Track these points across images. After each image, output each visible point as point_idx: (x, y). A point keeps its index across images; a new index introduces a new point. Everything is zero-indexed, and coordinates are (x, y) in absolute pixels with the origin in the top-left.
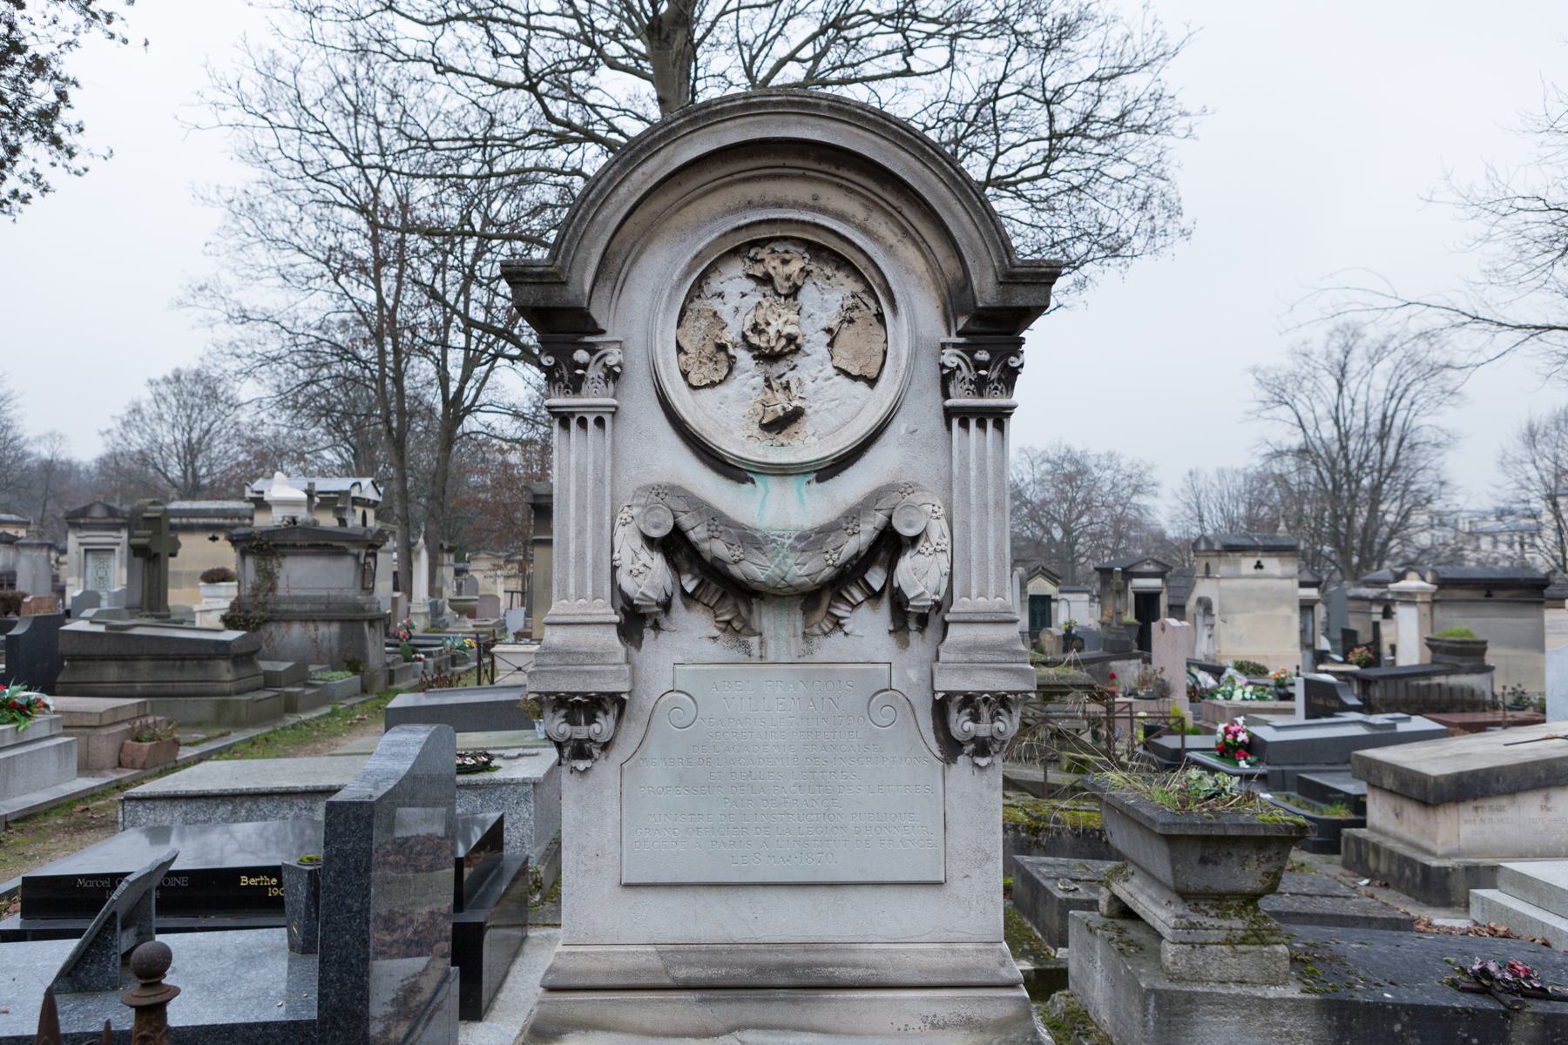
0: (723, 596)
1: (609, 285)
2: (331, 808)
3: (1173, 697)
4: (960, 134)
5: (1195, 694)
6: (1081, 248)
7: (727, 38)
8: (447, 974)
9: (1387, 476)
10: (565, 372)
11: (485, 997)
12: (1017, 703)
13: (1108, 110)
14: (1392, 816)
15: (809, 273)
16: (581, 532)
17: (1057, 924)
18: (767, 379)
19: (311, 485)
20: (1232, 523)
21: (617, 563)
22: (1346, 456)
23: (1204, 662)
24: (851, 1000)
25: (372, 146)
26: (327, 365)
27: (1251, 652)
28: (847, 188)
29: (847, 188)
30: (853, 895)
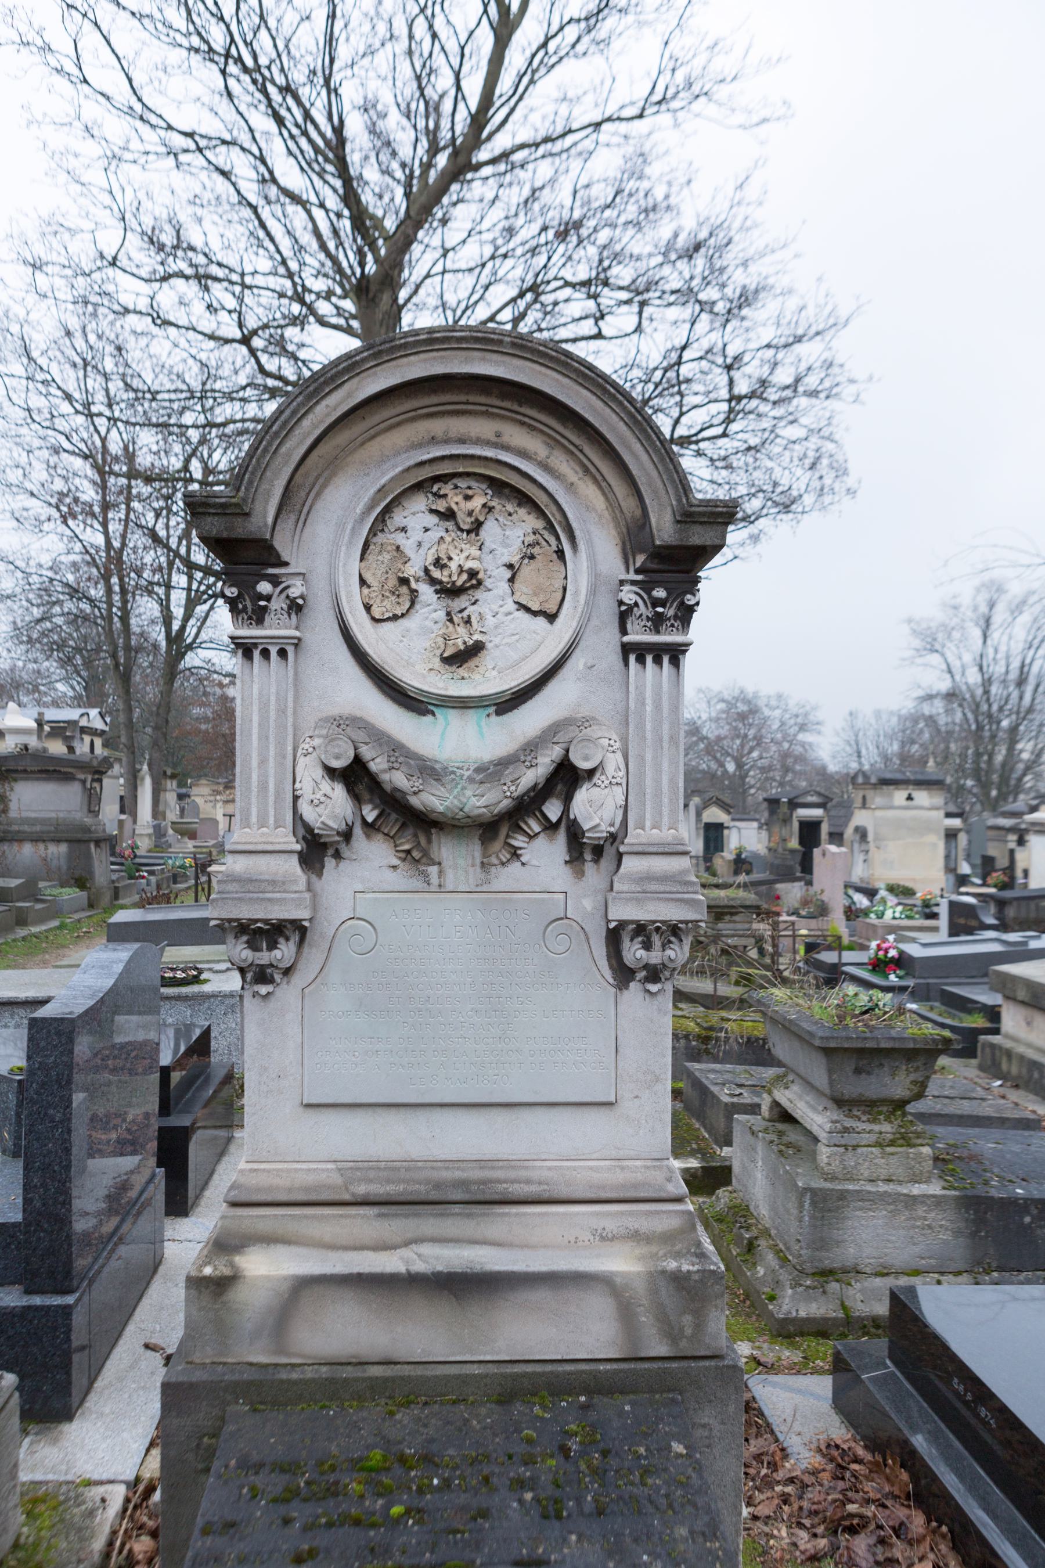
0: (403, 826)
1: (293, 517)
2: (34, 1023)
3: (831, 916)
4: (647, 396)
5: (852, 913)
6: (756, 503)
7: (433, 301)
8: (153, 1176)
9: (1024, 719)
10: (248, 603)
11: (191, 1194)
12: (687, 932)
13: (783, 376)
14: (1024, 1024)
15: (491, 509)
16: (263, 762)
17: (722, 1125)
18: (448, 614)
19: (41, 714)
20: (886, 759)
21: (298, 793)
22: (988, 700)
23: (860, 884)
24: (524, 1214)
25: (100, 397)
26: (59, 602)
27: (901, 876)
28: (529, 426)
29: (529, 426)
30: (526, 1114)
